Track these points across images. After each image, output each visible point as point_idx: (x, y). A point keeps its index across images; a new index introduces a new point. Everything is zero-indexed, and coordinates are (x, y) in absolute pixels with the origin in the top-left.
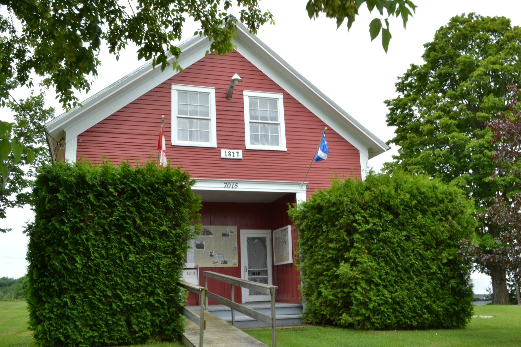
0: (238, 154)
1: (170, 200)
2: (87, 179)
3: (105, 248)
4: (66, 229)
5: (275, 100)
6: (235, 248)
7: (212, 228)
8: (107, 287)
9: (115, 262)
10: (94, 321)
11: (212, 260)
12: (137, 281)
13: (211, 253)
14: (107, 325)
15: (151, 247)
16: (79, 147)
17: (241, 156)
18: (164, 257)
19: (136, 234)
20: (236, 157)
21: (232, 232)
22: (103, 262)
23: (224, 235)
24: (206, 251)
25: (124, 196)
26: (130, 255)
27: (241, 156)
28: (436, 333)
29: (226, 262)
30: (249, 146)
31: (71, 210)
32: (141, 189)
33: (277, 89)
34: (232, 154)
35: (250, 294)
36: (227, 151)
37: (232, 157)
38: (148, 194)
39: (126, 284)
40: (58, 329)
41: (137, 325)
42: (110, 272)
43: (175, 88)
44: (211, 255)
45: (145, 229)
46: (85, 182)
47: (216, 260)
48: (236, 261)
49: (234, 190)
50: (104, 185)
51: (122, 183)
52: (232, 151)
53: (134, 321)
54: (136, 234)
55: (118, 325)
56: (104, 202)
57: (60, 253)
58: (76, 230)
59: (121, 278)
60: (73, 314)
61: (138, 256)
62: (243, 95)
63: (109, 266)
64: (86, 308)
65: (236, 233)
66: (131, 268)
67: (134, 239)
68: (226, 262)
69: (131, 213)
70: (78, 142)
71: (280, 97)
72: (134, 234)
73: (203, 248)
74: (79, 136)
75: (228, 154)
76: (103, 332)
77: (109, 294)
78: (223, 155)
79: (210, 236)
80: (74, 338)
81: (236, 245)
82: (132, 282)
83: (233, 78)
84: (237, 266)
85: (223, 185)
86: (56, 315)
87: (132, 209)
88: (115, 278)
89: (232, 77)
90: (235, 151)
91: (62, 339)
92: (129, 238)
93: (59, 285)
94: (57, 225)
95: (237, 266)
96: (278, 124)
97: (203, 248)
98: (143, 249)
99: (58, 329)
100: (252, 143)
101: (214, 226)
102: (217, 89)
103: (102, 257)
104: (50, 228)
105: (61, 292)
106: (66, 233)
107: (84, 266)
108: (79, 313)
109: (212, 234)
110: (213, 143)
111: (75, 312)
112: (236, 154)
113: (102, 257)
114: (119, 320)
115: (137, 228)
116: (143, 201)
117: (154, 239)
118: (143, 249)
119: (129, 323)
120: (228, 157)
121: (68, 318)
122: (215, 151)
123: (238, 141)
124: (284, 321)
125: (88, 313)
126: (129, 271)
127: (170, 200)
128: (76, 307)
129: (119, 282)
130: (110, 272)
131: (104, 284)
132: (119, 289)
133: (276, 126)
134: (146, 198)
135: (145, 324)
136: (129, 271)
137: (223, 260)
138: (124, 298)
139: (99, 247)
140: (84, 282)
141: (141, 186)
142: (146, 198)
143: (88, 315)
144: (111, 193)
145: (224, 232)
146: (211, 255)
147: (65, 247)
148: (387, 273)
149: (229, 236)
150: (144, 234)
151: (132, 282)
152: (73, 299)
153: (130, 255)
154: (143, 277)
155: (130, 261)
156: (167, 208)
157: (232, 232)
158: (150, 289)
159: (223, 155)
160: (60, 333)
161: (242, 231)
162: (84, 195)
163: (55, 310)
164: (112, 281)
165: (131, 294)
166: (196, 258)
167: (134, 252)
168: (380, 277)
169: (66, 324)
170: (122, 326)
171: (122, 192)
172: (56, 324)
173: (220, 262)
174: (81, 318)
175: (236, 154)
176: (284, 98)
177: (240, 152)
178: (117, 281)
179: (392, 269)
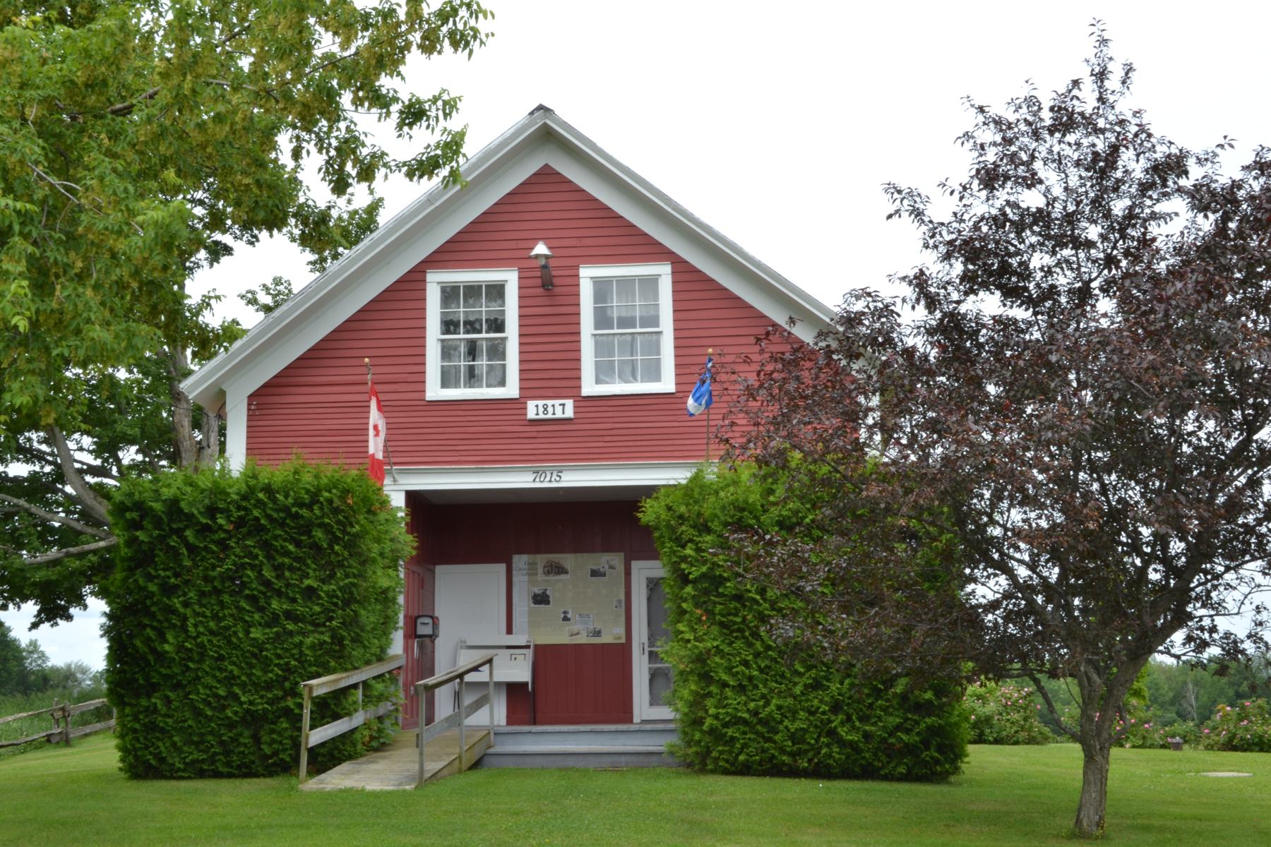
0: (564, 409)
1: (319, 534)
2: (183, 504)
3: (215, 617)
4: (153, 587)
5: (652, 281)
6: (620, 601)
7: (568, 560)
8: (219, 681)
9: (229, 642)
10: (201, 735)
11: (568, 628)
12: (266, 672)
13: (565, 612)
14: (222, 743)
15: (289, 615)
16: (250, 417)
17: (569, 413)
18: (313, 632)
19: (264, 594)
20: (559, 415)
21: (611, 567)
22: (210, 641)
23: (595, 573)
24: (554, 609)
25: (244, 530)
26: (253, 630)
27: (569, 413)
28: (767, 780)
29: (597, 633)
30: (589, 387)
31: (161, 556)
32: (269, 517)
33: (656, 252)
34: (550, 410)
35: (651, 704)
36: (541, 403)
37: (550, 416)
38: (282, 525)
39: (249, 675)
40: (147, 747)
41: (270, 745)
42: (221, 658)
43: (435, 281)
44: (566, 619)
45: (278, 584)
46: (181, 511)
47: (576, 628)
48: (621, 631)
49: (554, 485)
50: (212, 511)
51: (239, 508)
52: (550, 402)
53: (265, 738)
54: (264, 594)
55: (239, 744)
56: (213, 541)
57: (145, 627)
58: (168, 590)
59: (241, 668)
60: (166, 723)
61: (267, 631)
62: (577, 276)
63: (219, 647)
64: (187, 714)
65: (621, 568)
66: (256, 650)
67: (262, 602)
68: (597, 633)
69: (256, 557)
70: (249, 410)
71: (664, 271)
72: (260, 592)
73: (547, 602)
74: (250, 397)
75: (541, 410)
76: (215, 754)
77: (222, 692)
78: (531, 414)
79: (563, 577)
80: (171, 761)
81: (622, 597)
82: (259, 673)
83: (534, 252)
84: (623, 641)
85: (530, 477)
86: (145, 725)
87: (256, 551)
88: (230, 668)
89: (532, 249)
90: (557, 402)
91: (153, 762)
92: (252, 599)
93: (147, 679)
94: (141, 581)
95: (623, 641)
96: (660, 333)
97: (547, 602)
98: (274, 620)
99: (147, 747)
100: (598, 381)
101: (573, 555)
102: (521, 270)
103: (212, 633)
104: (131, 586)
105: (152, 688)
106: (152, 595)
107: (180, 648)
108: (177, 722)
109: (567, 573)
110: (511, 389)
111: (169, 720)
112: (559, 410)
113: (212, 633)
114: (241, 735)
115: (267, 584)
116: (276, 538)
117: (294, 600)
118: (274, 620)
119: (256, 739)
120: (541, 416)
121: (162, 730)
122: (516, 405)
123: (567, 383)
124: (642, 758)
125: (190, 722)
126: (254, 655)
127: (319, 534)
128: (171, 713)
129: (236, 672)
130: (221, 658)
131: (214, 676)
132: (238, 685)
133: (654, 337)
134: (278, 532)
135: (281, 743)
136: (254, 655)
137: (591, 627)
138: (243, 699)
139: (205, 617)
140: (183, 673)
141: (269, 512)
142: (278, 532)
143: (190, 726)
144: (221, 527)
145: (594, 567)
146: (566, 619)
147: (153, 616)
148: (746, 663)
149: (604, 575)
150: (279, 594)
151: (259, 673)
152: (168, 701)
153: (253, 630)
154: (276, 665)
155: (253, 639)
156: (316, 547)
157: (611, 567)
158: (287, 685)
159: (531, 414)
160: (151, 753)
161: (636, 565)
162: (179, 533)
163: (141, 717)
164: (226, 670)
165: (257, 692)
166: (533, 624)
167: (260, 624)
168: (729, 670)
169: (158, 739)
170: (245, 745)
171: (240, 523)
172: (146, 738)
173: (584, 634)
174: (181, 730)
175: (559, 410)
176: (673, 272)
177: (569, 403)
178: (231, 671)
179: (757, 655)
